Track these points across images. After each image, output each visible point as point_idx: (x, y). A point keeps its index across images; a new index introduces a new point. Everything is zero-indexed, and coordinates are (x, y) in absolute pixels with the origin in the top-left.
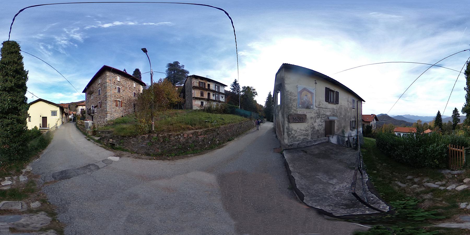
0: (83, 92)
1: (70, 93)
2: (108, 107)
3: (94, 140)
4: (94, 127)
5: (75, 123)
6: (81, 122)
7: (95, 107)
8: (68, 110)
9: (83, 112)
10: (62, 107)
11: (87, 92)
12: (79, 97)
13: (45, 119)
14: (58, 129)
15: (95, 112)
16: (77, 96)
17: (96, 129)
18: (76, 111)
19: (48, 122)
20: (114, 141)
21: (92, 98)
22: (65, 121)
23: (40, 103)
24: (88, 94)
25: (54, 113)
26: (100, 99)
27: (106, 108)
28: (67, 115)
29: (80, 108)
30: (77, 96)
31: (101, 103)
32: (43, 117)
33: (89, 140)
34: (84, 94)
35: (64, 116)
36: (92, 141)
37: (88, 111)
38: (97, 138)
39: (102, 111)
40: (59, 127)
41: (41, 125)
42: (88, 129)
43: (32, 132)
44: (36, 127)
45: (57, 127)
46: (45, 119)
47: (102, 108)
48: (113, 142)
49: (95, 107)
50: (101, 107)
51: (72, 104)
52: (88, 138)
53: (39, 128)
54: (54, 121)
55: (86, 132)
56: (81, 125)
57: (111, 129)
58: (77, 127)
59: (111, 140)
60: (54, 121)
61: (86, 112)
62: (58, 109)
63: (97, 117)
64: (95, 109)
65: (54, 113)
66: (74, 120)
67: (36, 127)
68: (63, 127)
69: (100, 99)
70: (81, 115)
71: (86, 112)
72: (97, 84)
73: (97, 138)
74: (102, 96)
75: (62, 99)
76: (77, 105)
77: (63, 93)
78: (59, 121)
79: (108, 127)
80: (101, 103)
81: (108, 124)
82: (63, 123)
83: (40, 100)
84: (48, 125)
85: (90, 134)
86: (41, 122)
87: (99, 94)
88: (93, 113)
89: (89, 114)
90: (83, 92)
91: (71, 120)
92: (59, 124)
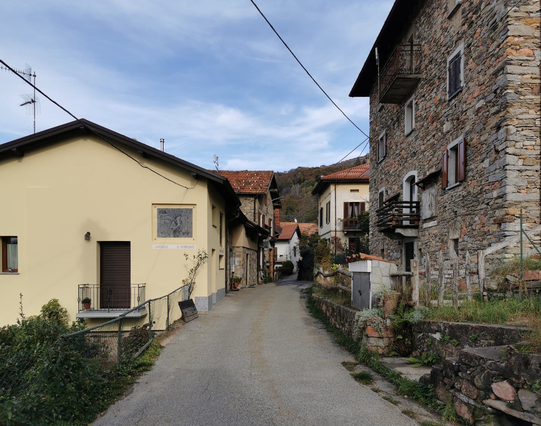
0: (356, 92)
1: (285, 109)
2: (512, 177)
3: (394, 380)
4: (405, 304)
5: (306, 286)
6: (335, 274)
7: (427, 182)
8: (269, 209)
9: (356, 221)
10: (223, 191)
11: (380, 87)
12: (338, 133)
13: (114, 257)
14: (195, 315)
15: (426, 213)
16: (326, 129)
17: (416, 316)
18: (316, 216)
19: (138, 275)
20: (528, 399)
21: (408, 123)
22: (252, 276)
23: (84, 150)
24: (385, 100)
25: (174, 222)
26: (459, 123)
27: (501, 182)
28: (258, 235)
29: (340, 197)
30: (326, 129)
31: (466, 153)
32: (104, 246)
33: (363, 378)
34: (363, 104)
35: (242, 239)
36: (380, 384)
37: (380, 212)
38: (414, 374)
39: (471, 202)
40: (201, 307)
41: (94, 296)
42: (365, 314)
43: (22, 337)
44: (53, 311)
45: (187, 305)
46: (114, 257)
47: (473, 186)
48: (516, 405)
49: (427, 182)
50: (461, 180)
51: (300, 176)
52: (360, 369)
53: (73, 311)
54: (171, 269)
55: (355, 334)
56: (332, 291)
57: (518, 321)
58: (314, 308)
59: (503, 389)
60: (171, 269)
61: (373, 219)
62: (199, 198)
63: (434, 244)
64: (428, 198)
65: (174, 222)
66: (303, 270)
67: (53, 311)
68: (230, 307)
69: (459, 123)
70: (344, 241)
71: (373, 219)
72: (439, 18)
73: (414, 374)
74: (473, 99)
75: (236, 147)
76: (321, 181)
77: (245, 108)
78: (203, 270)
79: (500, 307)
80: (466, 153)
81: (504, 287)
82: (232, 285)
83: (80, 130)
84: (134, 292)
85: (376, 343)
86: (92, 277)
87: (455, 89)
88: (416, 220)
89: (389, 232)
90: (356, 92)
91: (286, 269)
92: (207, 285)
